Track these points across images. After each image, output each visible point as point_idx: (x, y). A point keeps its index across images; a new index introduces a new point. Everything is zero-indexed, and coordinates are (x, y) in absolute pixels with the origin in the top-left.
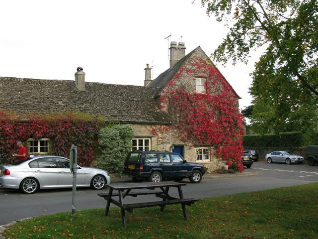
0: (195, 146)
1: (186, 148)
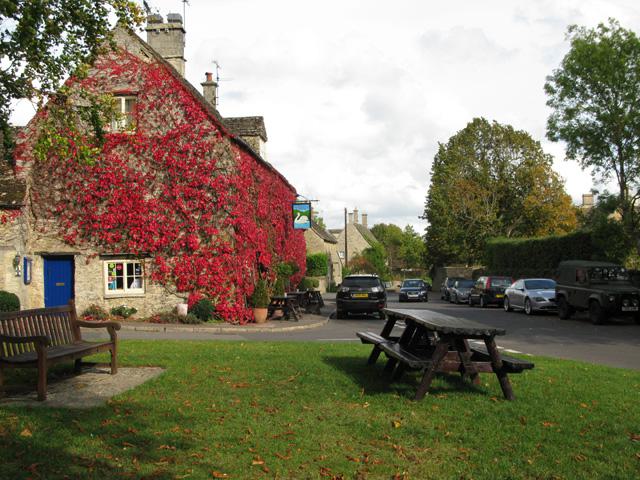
1: (78, 261)
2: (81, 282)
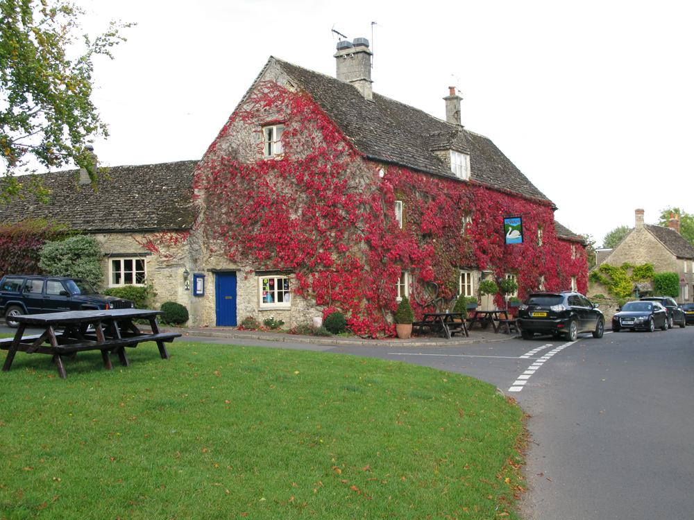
0: (259, 273)
1: (239, 276)
2: (241, 296)
